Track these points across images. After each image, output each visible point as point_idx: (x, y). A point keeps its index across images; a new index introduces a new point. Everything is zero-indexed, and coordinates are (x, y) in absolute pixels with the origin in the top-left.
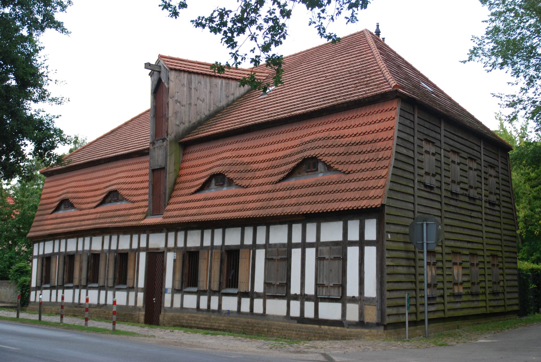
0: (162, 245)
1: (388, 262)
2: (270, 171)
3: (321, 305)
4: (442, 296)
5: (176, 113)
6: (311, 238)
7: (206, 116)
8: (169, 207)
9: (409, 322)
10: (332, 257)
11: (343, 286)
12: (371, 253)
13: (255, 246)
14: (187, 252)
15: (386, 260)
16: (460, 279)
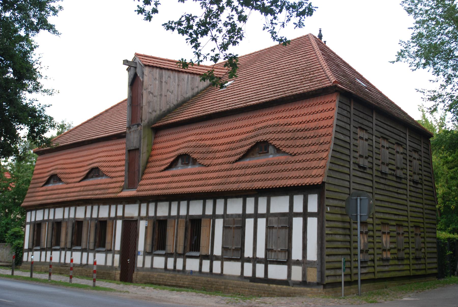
0: (136, 214)
1: (327, 231)
3: (270, 267)
5: (149, 103)
7: (174, 105)
10: (280, 226)
11: (289, 251)
12: (313, 223)
13: (214, 216)
15: (326, 229)
16: (388, 246)
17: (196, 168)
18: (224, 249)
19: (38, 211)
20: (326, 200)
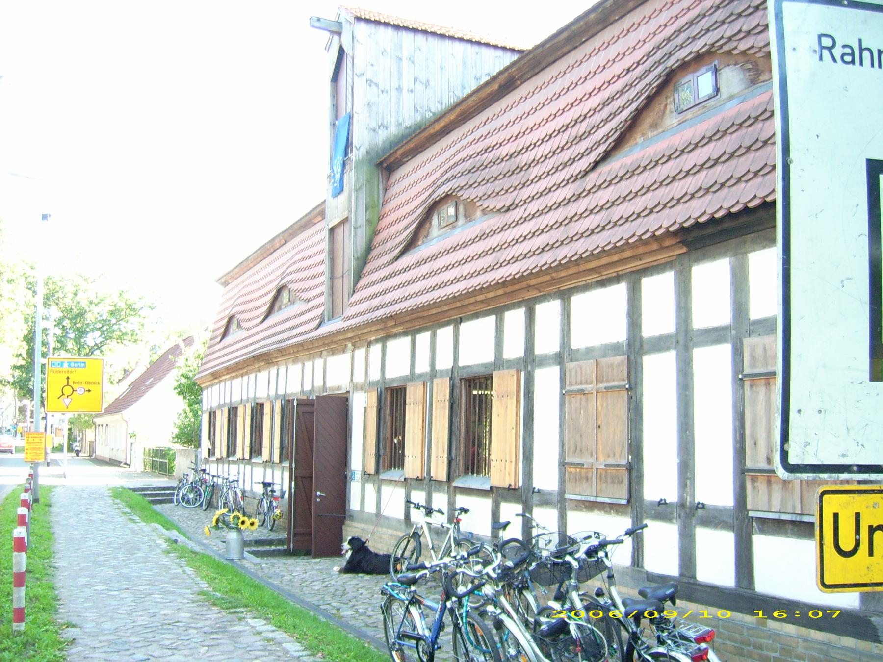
7: (434, 114)
14: (386, 389)
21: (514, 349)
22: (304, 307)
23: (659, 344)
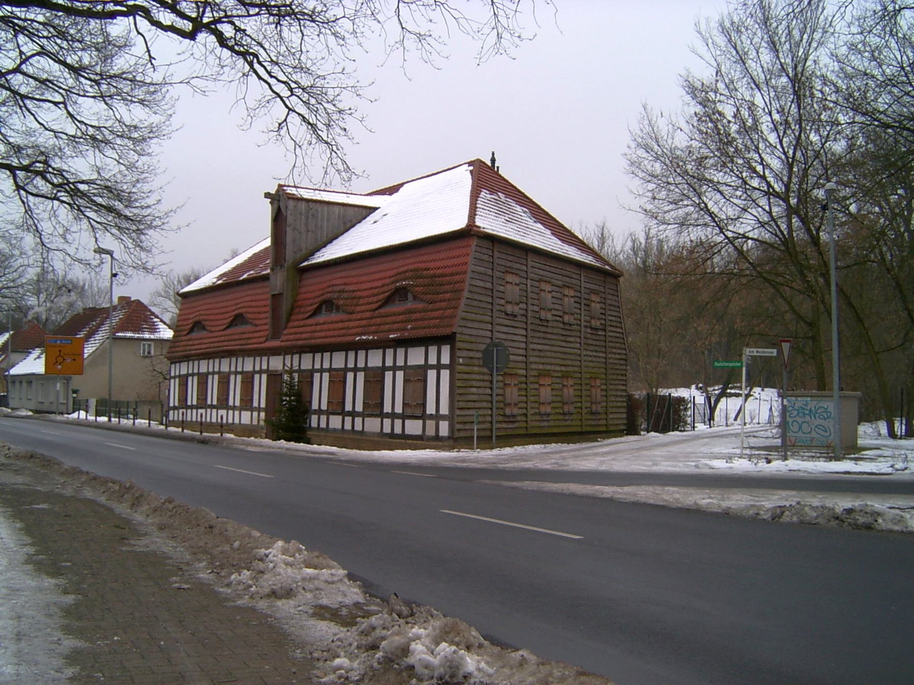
0: (280, 368)
1: (459, 384)
2: (371, 300)
3: (407, 422)
4: (526, 415)
5: (294, 240)
6: (361, 364)
8: (285, 332)
9: (477, 437)
11: (424, 405)
12: (445, 374)
15: (457, 382)
16: (550, 399)
17: (341, 316)
18: (365, 404)
19: (303, 355)
20: (458, 351)
21: (351, 365)
22: (254, 329)
23: (432, 367)
